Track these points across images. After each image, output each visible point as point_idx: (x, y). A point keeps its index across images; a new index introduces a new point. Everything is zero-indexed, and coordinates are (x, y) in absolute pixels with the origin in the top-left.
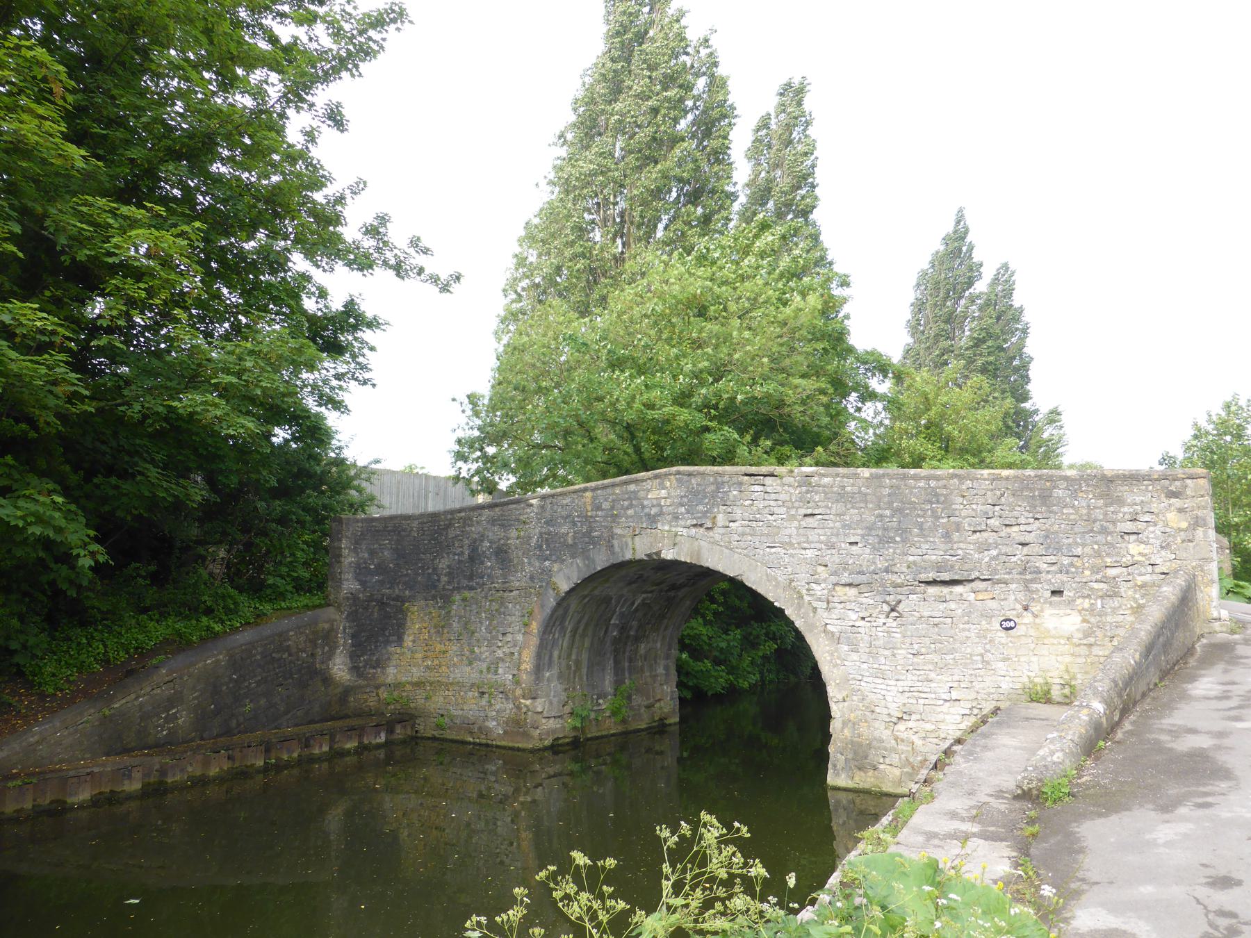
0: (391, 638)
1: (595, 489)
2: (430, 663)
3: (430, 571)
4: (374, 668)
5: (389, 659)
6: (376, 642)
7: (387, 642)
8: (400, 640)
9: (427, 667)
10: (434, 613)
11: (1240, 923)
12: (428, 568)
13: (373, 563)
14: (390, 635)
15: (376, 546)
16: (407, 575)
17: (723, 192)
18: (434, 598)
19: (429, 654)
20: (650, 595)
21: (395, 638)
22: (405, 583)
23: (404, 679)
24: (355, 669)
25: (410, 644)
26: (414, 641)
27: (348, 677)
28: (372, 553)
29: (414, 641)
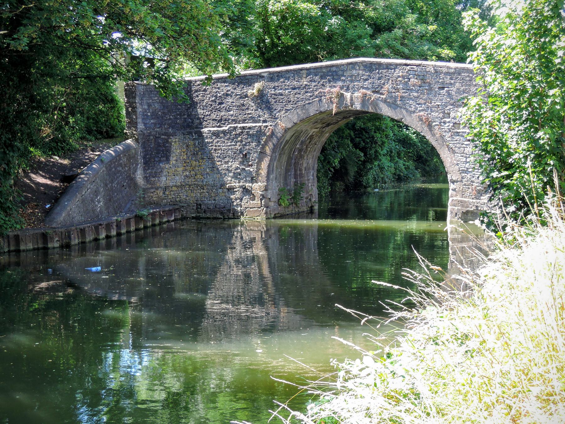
0: (162, 159)
1: (273, 77)
2: (188, 173)
3: (186, 116)
4: (154, 177)
5: (162, 171)
6: (154, 161)
7: (160, 161)
8: (168, 160)
9: (186, 176)
10: (191, 143)
11: (266, 291)
12: (184, 115)
13: (149, 112)
14: (162, 157)
15: (151, 101)
16: (170, 119)
17: (121, 32)
18: (190, 133)
19: (187, 168)
20: (316, 130)
21: (165, 159)
22: (169, 124)
23: (171, 184)
24: (146, 178)
25: (174, 162)
26: (176, 161)
27: (143, 183)
28: (149, 105)
29: (176, 161)
